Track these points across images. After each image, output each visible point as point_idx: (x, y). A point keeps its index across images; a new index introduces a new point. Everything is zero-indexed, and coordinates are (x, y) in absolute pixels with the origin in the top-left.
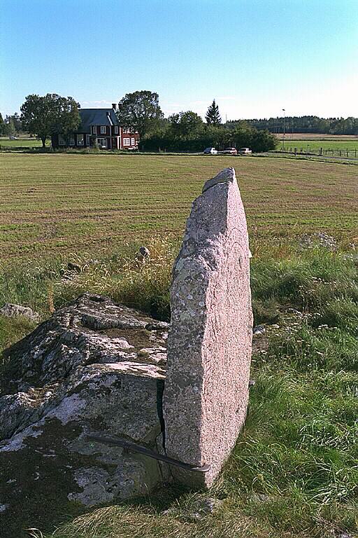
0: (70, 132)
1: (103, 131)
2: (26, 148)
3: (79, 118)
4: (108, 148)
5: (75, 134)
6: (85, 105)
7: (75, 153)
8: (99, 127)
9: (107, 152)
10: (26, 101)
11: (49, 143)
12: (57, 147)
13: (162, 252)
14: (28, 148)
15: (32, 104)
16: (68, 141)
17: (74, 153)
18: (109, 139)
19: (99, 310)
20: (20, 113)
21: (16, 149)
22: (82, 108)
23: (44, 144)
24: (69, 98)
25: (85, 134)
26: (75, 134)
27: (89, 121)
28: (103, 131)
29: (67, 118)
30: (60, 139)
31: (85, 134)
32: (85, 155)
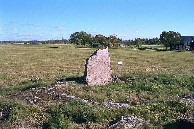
0: (177, 44)
1: (189, 44)
2: (159, 49)
3: (180, 39)
4: (191, 50)
5: (178, 45)
6: (182, 35)
7: (176, 51)
8: (187, 43)
9: (189, 51)
10: (162, 33)
11: (169, 48)
12: (171, 49)
13: (81, 75)
14: (160, 49)
15: (164, 34)
16: (175, 47)
17: (175, 51)
18: (191, 47)
19: (22, 92)
20: (159, 38)
21: (158, 49)
22: (182, 36)
23: (167, 48)
24: (177, 32)
25: (182, 45)
26: (178, 45)
27: (184, 40)
28: (189, 44)
29: (175, 39)
30: (173, 47)
31: (182, 45)
32: (179, 52)
